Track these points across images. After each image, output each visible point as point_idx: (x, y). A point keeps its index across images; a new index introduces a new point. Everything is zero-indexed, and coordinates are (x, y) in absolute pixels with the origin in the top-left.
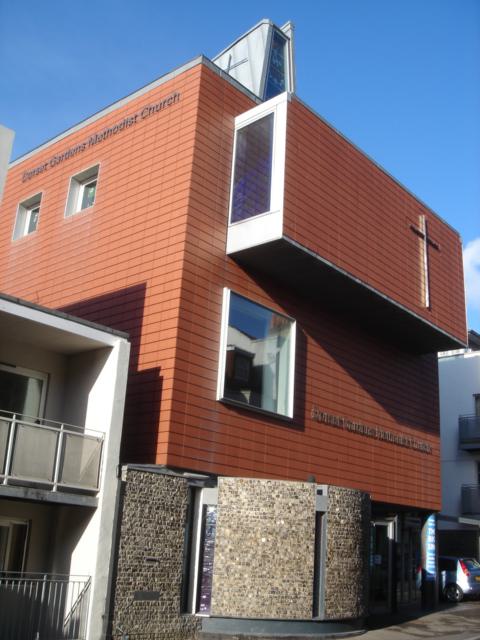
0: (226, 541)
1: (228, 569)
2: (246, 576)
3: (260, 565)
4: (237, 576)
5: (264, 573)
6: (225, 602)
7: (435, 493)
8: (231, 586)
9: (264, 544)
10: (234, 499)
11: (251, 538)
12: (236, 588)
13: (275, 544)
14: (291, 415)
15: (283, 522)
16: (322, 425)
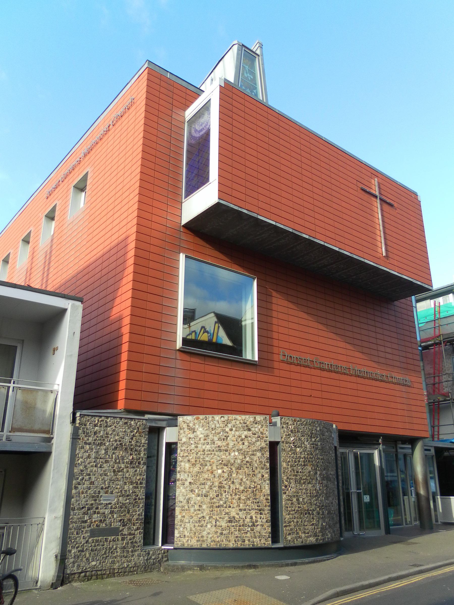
0: (186, 475)
1: (188, 501)
2: (204, 507)
3: (217, 496)
4: (197, 507)
5: (221, 502)
6: (186, 534)
8: (192, 517)
9: (220, 476)
10: (192, 436)
12: (195, 518)
13: (230, 473)
14: (256, 359)
15: (237, 453)
16: (292, 366)
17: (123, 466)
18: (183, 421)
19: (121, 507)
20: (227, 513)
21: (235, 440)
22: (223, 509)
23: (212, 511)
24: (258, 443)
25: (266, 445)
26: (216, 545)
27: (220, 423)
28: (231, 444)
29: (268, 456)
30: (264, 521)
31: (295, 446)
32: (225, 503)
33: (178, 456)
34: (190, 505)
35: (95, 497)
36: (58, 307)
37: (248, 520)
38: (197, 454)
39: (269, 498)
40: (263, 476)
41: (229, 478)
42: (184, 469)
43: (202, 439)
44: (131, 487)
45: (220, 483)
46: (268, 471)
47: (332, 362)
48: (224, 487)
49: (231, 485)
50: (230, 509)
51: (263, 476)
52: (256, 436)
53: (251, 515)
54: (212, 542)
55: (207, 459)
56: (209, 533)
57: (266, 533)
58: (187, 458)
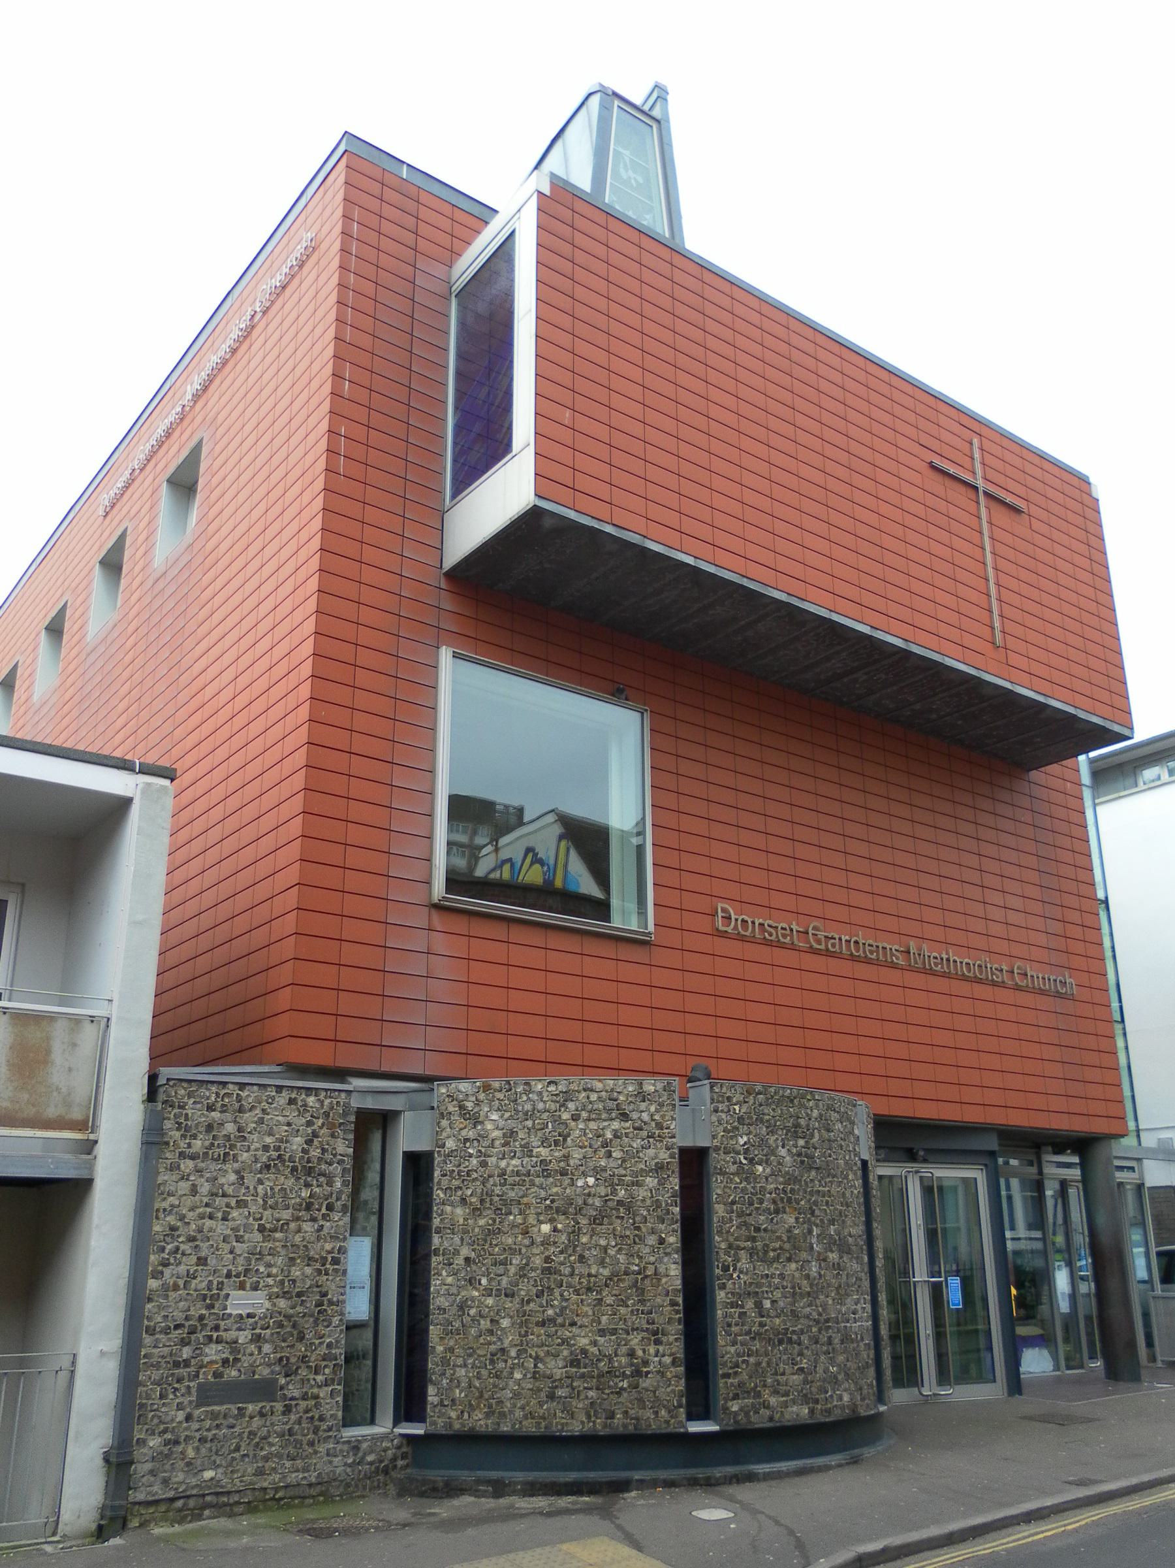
0: (457, 1239)
1: (462, 1307)
2: (505, 1323)
7: (381, 727)
9: (546, 1243)
10: (471, 1134)
11: (513, 1226)
13: (576, 1232)
15: (591, 1181)
18: (448, 1096)
20: (564, 1341)
28: (577, 1154)
30: (667, 1360)
31: (751, 1161)
35: (211, 1299)
40: (662, 1241)
43: (497, 1143)
46: (677, 1226)
48: (557, 1272)
50: (574, 1329)
51: (662, 1241)
58: (460, 1193)
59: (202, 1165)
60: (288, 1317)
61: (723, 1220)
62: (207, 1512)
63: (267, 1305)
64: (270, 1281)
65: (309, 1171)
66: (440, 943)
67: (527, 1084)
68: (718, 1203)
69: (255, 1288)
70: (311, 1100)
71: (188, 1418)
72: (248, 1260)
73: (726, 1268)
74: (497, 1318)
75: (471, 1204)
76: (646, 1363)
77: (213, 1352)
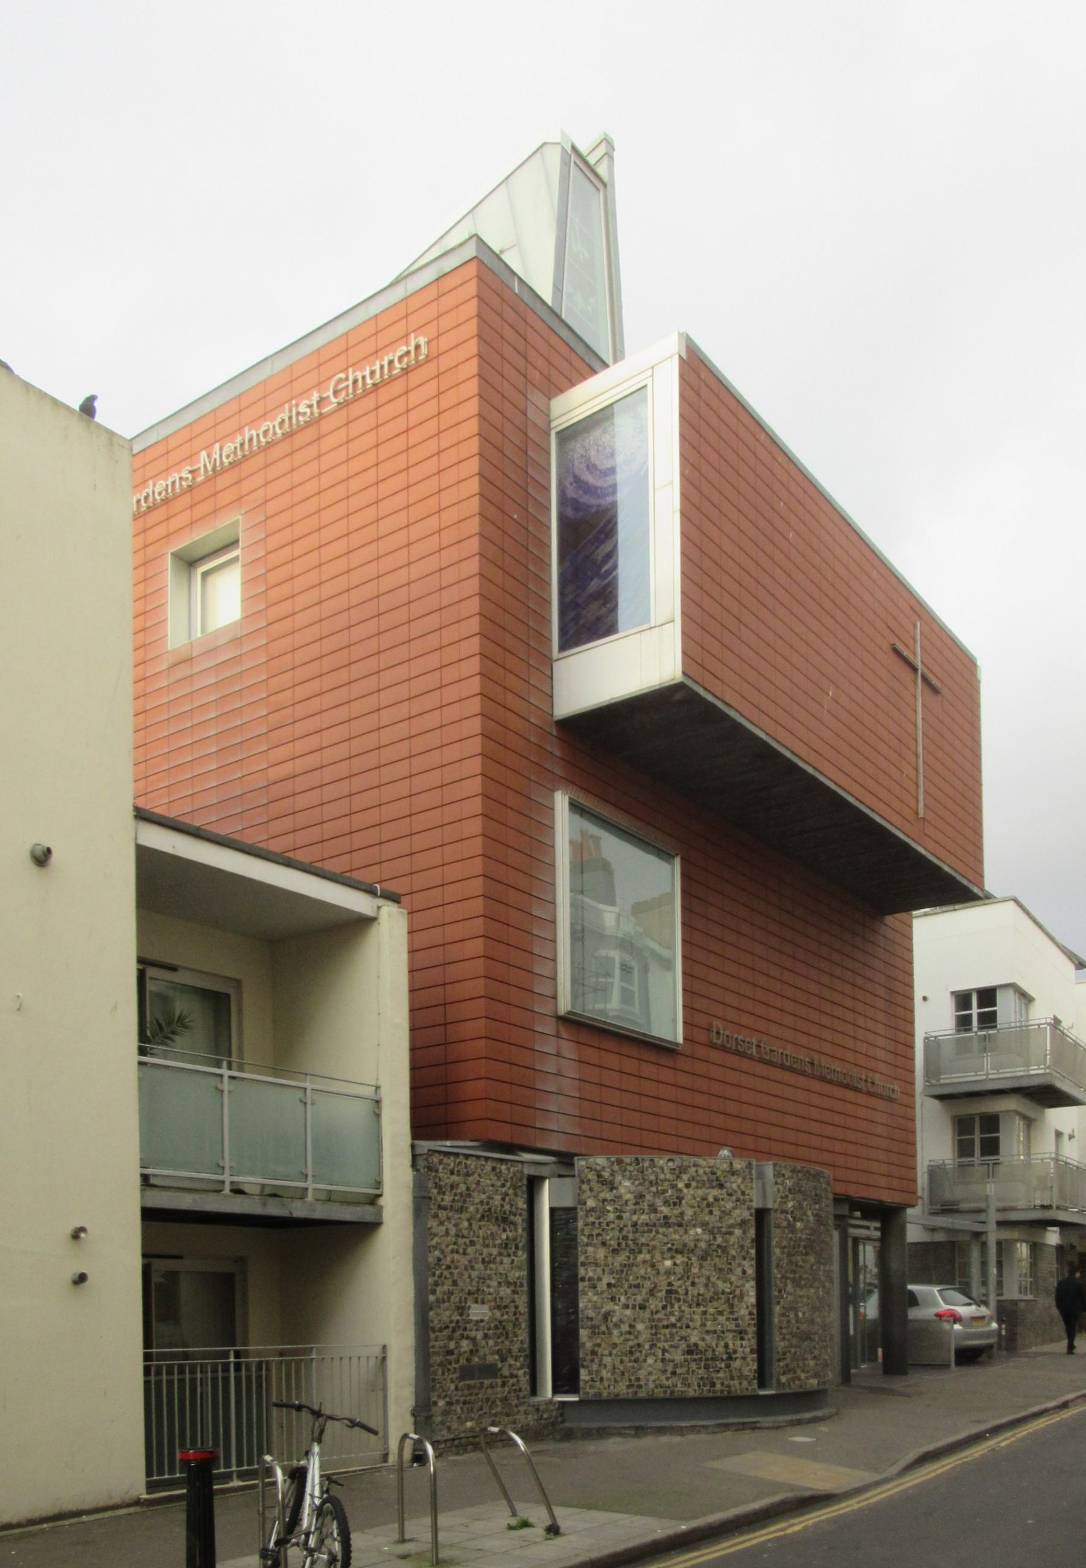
0: (599, 1270)
1: (607, 1316)
2: (640, 1327)
3: (664, 1307)
5: (673, 1319)
6: (604, 1373)
9: (668, 1273)
10: (609, 1196)
13: (688, 1266)
15: (699, 1231)
17: (495, 1251)
18: (588, 1168)
19: (496, 1328)
20: (682, 1338)
21: (696, 1205)
22: (674, 1330)
23: (656, 1334)
24: (737, 1212)
25: (751, 1215)
26: (665, 1392)
27: (666, 1171)
28: (689, 1213)
29: (754, 1236)
30: (748, 1350)
31: (794, 1219)
32: (679, 1320)
33: (579, 1234)
34: (611, 1325)
35: (462, 1309)
36: (347, 910)
37: (720, 1349)
38: (621, 1230)
39: (755, 1311)
40: (744, 1272)
41: (686, 1274)
42: (595, 1259)
43: (630, 1203)
44: (508, 1291)
45: (670, 1284)
46: (754, 1262)
47: (788, 1051)
48: (677, 1292)
49: (690, 1288)
50: (689, 1330)
51: (744, 1272)
52: (734, 1198)
53: (726, 1340)
54: (656, 1387)
55: (643, 1240)
56: (650, 1373)
57: (750, 1370)
58: (600, 1238)
59: (450, 1214)
60: (501, 1322)
61: (780, 1259)
62: (470, 1448)
63: (490, 1314)
64: (490, 1297)
65: (505, 1220)
66: (568, 1050)
67: (652, 1160)
68: (776, 1247)
69: (483, 1302)
70: (503, 1167)
71: (456, 1389)
72: (478, 1283)
73: (780, 1291)
74: (633, 1323)
75: (610, 1245)
76: (735, 1352)
77: (465, 1345)
